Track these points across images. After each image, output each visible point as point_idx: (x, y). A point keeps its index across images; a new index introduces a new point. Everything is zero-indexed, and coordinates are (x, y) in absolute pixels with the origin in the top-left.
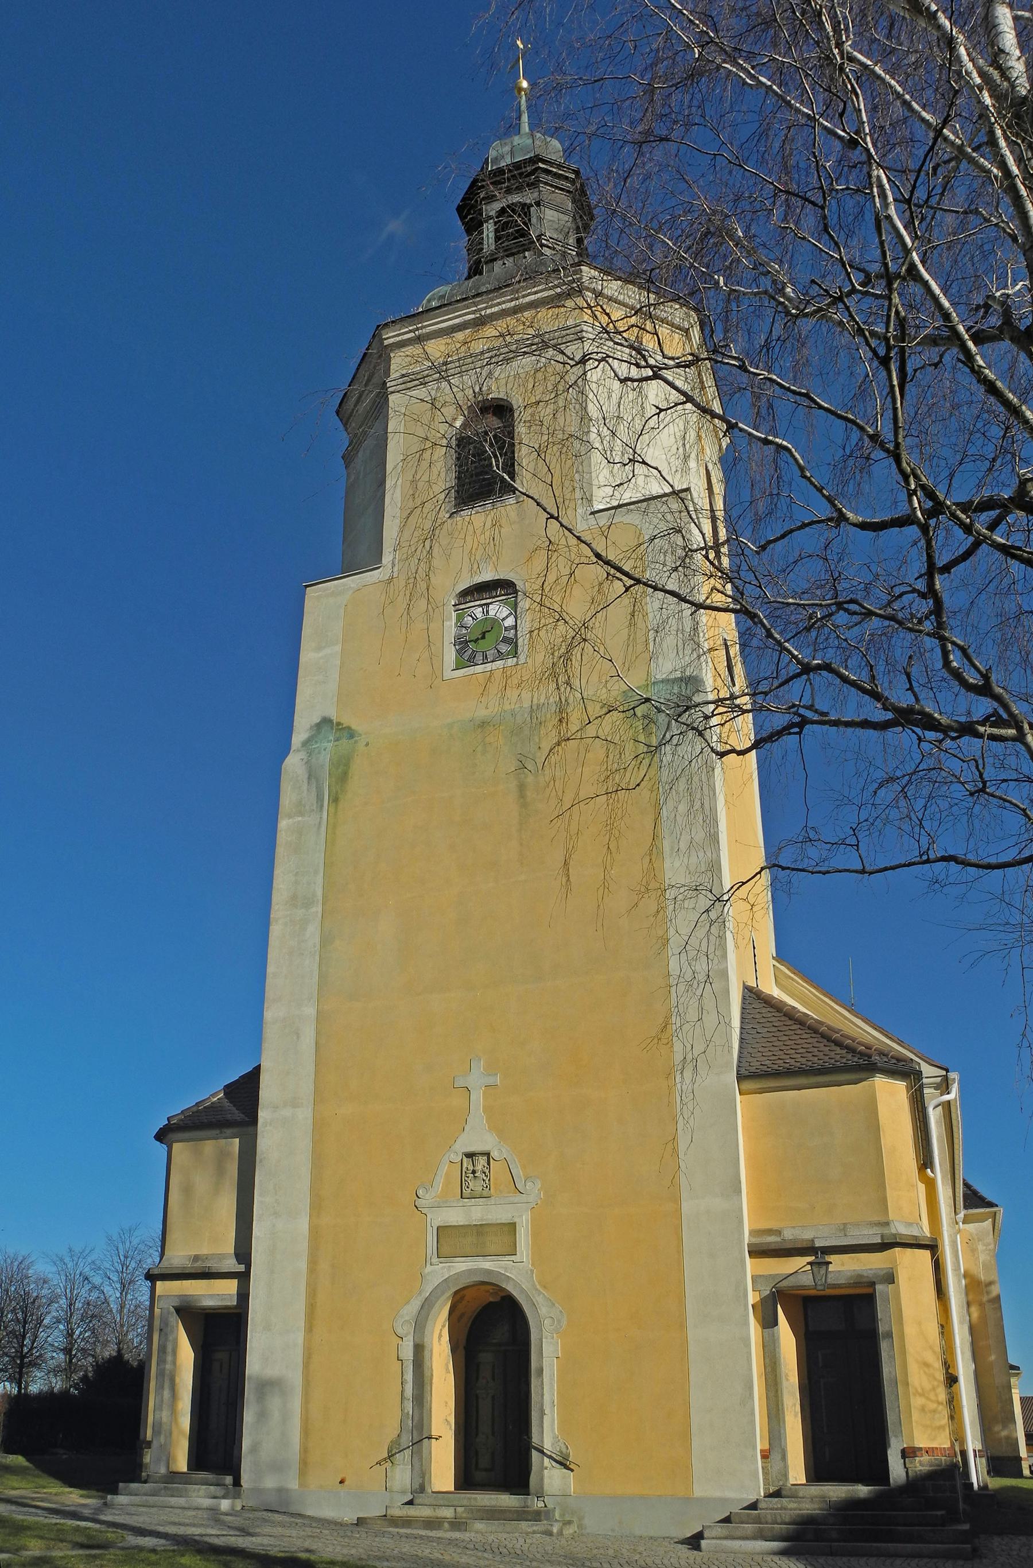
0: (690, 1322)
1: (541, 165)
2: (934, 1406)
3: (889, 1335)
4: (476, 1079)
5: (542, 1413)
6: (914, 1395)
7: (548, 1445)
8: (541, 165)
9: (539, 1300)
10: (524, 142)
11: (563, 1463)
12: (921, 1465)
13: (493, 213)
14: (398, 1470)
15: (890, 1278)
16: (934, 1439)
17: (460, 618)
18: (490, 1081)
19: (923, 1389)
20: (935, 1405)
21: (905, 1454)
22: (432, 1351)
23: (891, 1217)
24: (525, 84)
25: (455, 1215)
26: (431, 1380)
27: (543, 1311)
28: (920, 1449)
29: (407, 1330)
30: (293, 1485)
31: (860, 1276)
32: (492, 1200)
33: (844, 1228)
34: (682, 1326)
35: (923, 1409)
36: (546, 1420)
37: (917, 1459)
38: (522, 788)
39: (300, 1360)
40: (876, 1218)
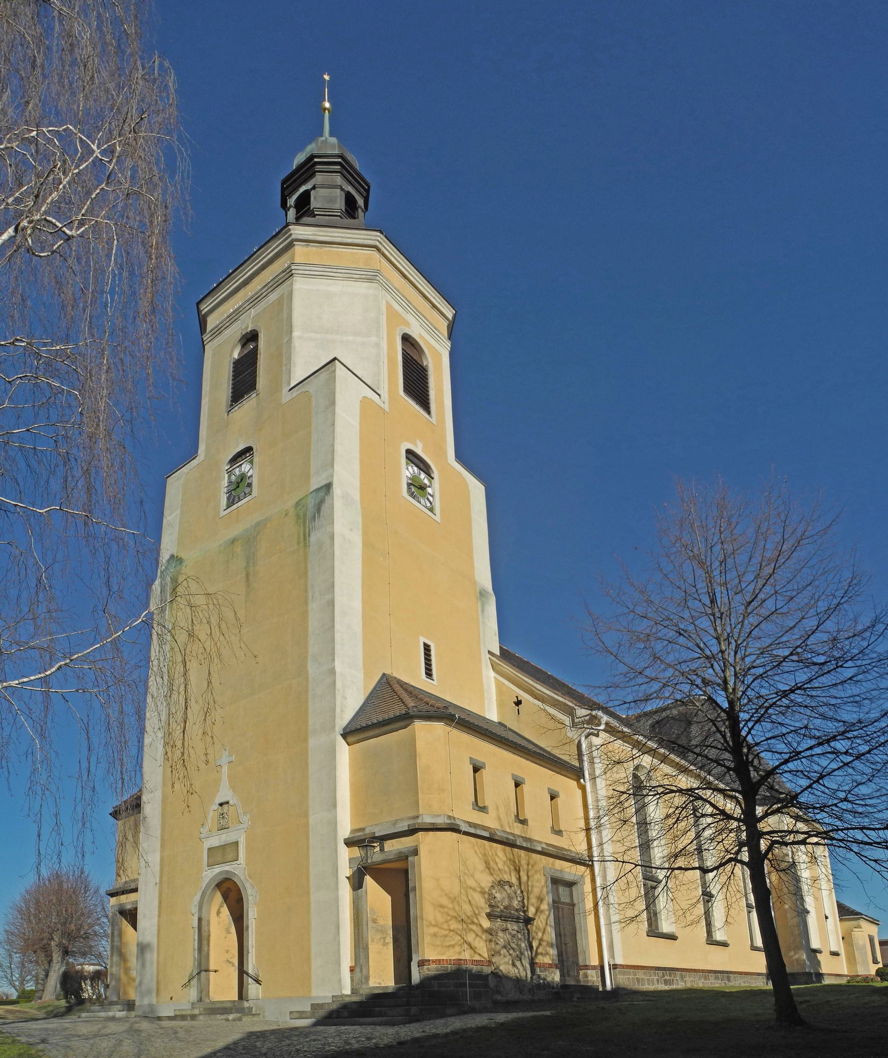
0: (312, 890)
1: (316, 160)
2: (444, 933)
3: (414, 889)
4: (224, 760)
5: (248, 952)
6: (429, 926)
7: (250, 972)
8: (316, 160)
9: (247, 885)
10: (328, 143)
11: (258, 981)
12: (431, 970)
13: (292, 204)
14: (192, 990)
15: (415, 852)
16: (444, 954)
17: (229, 477)
18: (230, 759)
19: (436, 922)
20: (447, 932)
21: (421, 963)
22: (209, 921)
23: (421, 811)
24: (327, 105)
25: (215, 841)
26: (209, 936)
27: (249, 891)
28: (429, 961)
29: (195, 910)
30: (154, 1001)
31: (401, 853)
32: (230, 830)
33: (395, 823)
34: (308, 893)
35: (435, 935)
36: (250, 955)
37: (425, 967)
38: (247, 575)
39: (156, 933)
40: (412, 814)
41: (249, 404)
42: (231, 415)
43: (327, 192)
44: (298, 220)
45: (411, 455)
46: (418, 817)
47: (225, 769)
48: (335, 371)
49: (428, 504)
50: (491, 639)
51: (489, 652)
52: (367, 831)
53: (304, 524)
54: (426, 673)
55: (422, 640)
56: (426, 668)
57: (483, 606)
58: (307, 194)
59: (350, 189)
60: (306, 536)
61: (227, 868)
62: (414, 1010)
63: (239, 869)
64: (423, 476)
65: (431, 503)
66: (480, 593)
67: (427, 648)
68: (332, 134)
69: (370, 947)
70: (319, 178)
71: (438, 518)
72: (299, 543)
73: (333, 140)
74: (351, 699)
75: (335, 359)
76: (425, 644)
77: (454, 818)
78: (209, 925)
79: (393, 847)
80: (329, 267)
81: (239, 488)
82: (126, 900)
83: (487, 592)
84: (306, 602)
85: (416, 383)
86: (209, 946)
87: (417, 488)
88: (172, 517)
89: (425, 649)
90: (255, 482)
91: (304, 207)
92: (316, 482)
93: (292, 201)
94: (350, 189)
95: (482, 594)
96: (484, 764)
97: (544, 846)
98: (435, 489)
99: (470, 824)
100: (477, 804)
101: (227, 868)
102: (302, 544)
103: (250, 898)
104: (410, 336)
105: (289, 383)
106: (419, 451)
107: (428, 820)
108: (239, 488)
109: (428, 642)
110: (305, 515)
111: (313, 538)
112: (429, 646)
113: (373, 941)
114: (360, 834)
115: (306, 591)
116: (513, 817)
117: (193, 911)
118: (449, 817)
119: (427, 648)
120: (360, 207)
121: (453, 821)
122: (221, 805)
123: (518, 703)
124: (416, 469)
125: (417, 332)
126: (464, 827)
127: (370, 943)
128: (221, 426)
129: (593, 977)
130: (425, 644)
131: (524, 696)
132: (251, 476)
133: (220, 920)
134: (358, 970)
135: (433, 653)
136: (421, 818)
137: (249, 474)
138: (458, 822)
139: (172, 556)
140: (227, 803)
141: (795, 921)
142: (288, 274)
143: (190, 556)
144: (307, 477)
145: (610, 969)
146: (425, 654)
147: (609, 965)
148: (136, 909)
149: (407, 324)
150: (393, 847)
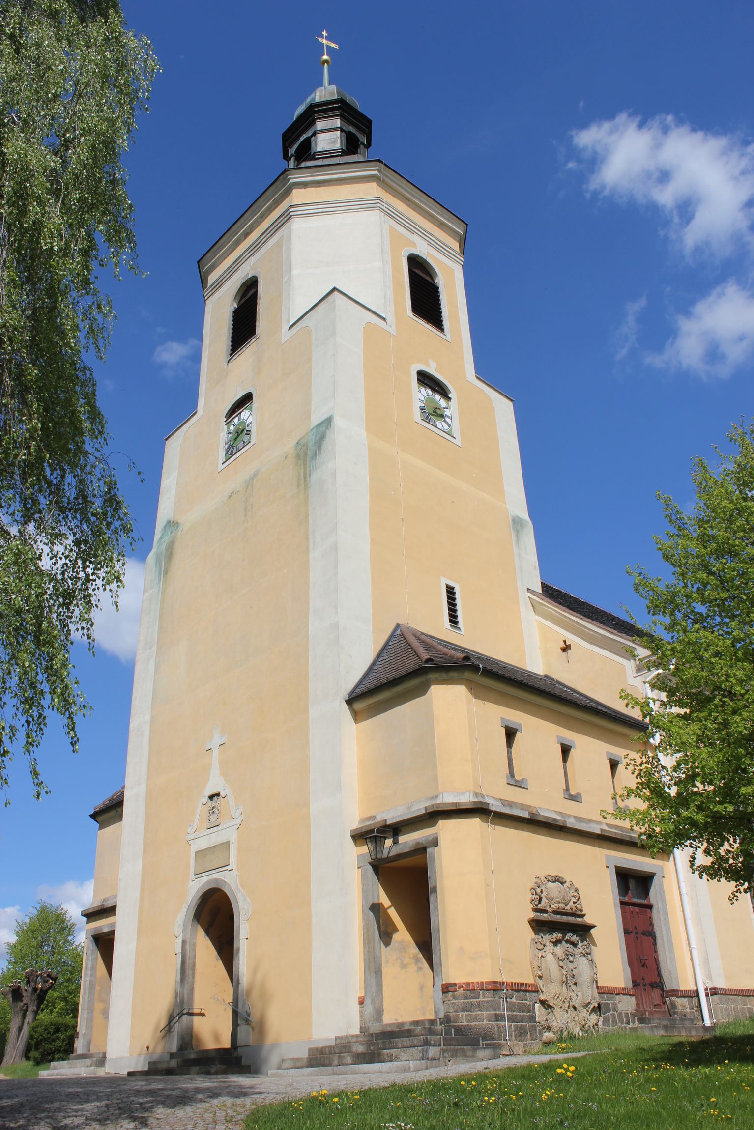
3: (435, 890)
10: (325, 92)
15: (435, 843)
17: (228, 428)
25: (203, 843)
26: (194, 966)
31: (418, 843)
41: (248, 352)
42: (230, 364)
43: (328, 137)
44: (297, 168)
45: (424, 378)
46: (437, 797)
47: (216, 753)
48: (334, 301)
49: (446, 427)
50: (532, 578)
51: (528, 589)
52: (379, 819)
53: (305, 464)
54: (451, 621)
55: (444, 581)
56: (450, 615)
57: (517, 536)
58: (308, 141)
59: (351, 129)
60: (306, 477)
61: (216, 875)
62: (433, 1051)
63: (232, 881)
64: (438, 397)
65: (449, 426)
66: (513, 520)
67: (451, 591)
68: (330, 84)
69: (384, 970)
70: (320, 125)
71: (458, 441)
72: (299, 486)
73: (333, 88)
74: (357, 658)
75: (334, 289)
76: (448, 587)
77: (483, 796)
78: (194, 950)
79: (408, 840)
80: (329, 203)
81: (239, 437)
82: (103, 924)
83: (521, 520)
84: (307, 551)
85: (425, 300)
86: (194, 977)
87: (433, 414)
88: (170, 482)
89: (448, 592)
90: (253, 429)
91: (305, 153)
92: (316, 418)
93: (292, 151)
94: (351, 129)
95: (517, 523)
96: (520, 725)
97: (605, 828)
98: (452, 409)
99: (503, 802)
100: (511, 773)
101: (216, 875)
102: (302, 486)
103: (242, 913)
104: (418, 256)
105: (289, 321)
106: (432, 371)
107: (449, 799)
108: (239, 437)
109: (452, 584)
110: (306, 454)
111: (314, 478)
112: (453, 588)
113: (387, 962)
114: (370, 822)
115: (307, 539)
116: (289, 446)
117: (177, 934)
118: (476, 795)
119: (451, 591)
120: (363, 144)
121: (481, 800)
122: (211, 797)
123: (566, 648)
124: (430, 392)
125: (423, 250)
126: (495, 806)
127: (383, 965)
128: (221, 376)
129: (683, 1006)
130: (448, 587)
131: (572, 639)
132: (250, 423)
133: (205, 949)
134: (368, 1002)
135: (457, 596)
136: (440, 797)
137: (248, 422)
138: (487, 800)
139: (169, 522)
140: (218, 795)
141: (645, 638)
142: (287, 217)
143: (188, 519)
144: (308, 414)
145: (707, 995)
146: (448, 598)
147: (706, 989)
148: (112, 933)
149: (414, 245)
150: (408, 840)
